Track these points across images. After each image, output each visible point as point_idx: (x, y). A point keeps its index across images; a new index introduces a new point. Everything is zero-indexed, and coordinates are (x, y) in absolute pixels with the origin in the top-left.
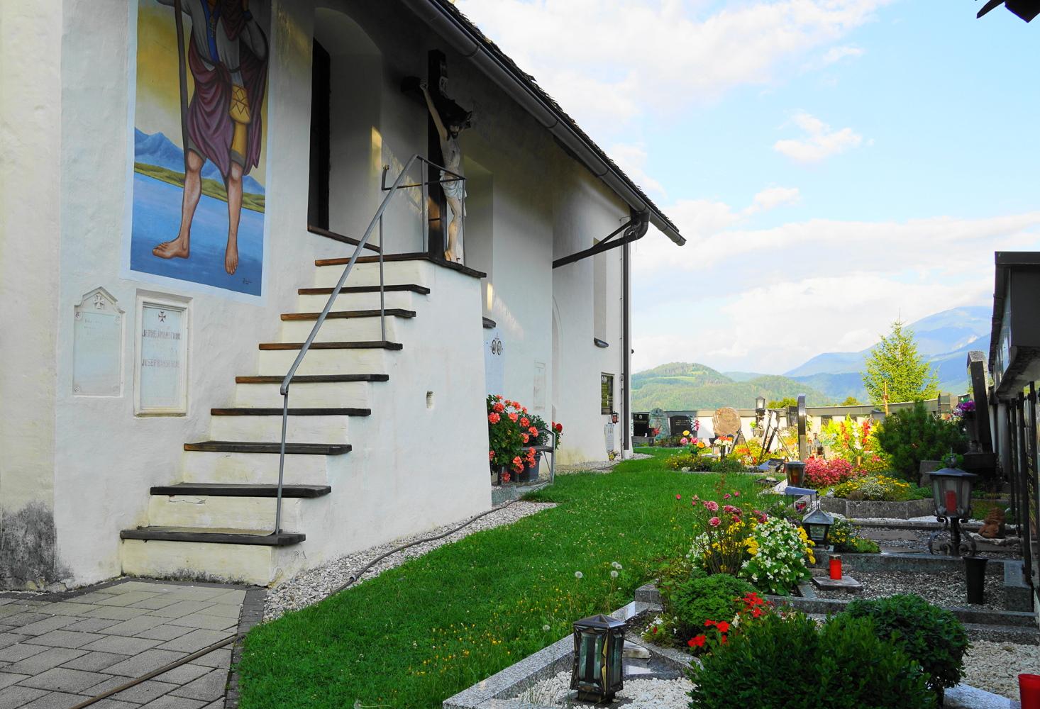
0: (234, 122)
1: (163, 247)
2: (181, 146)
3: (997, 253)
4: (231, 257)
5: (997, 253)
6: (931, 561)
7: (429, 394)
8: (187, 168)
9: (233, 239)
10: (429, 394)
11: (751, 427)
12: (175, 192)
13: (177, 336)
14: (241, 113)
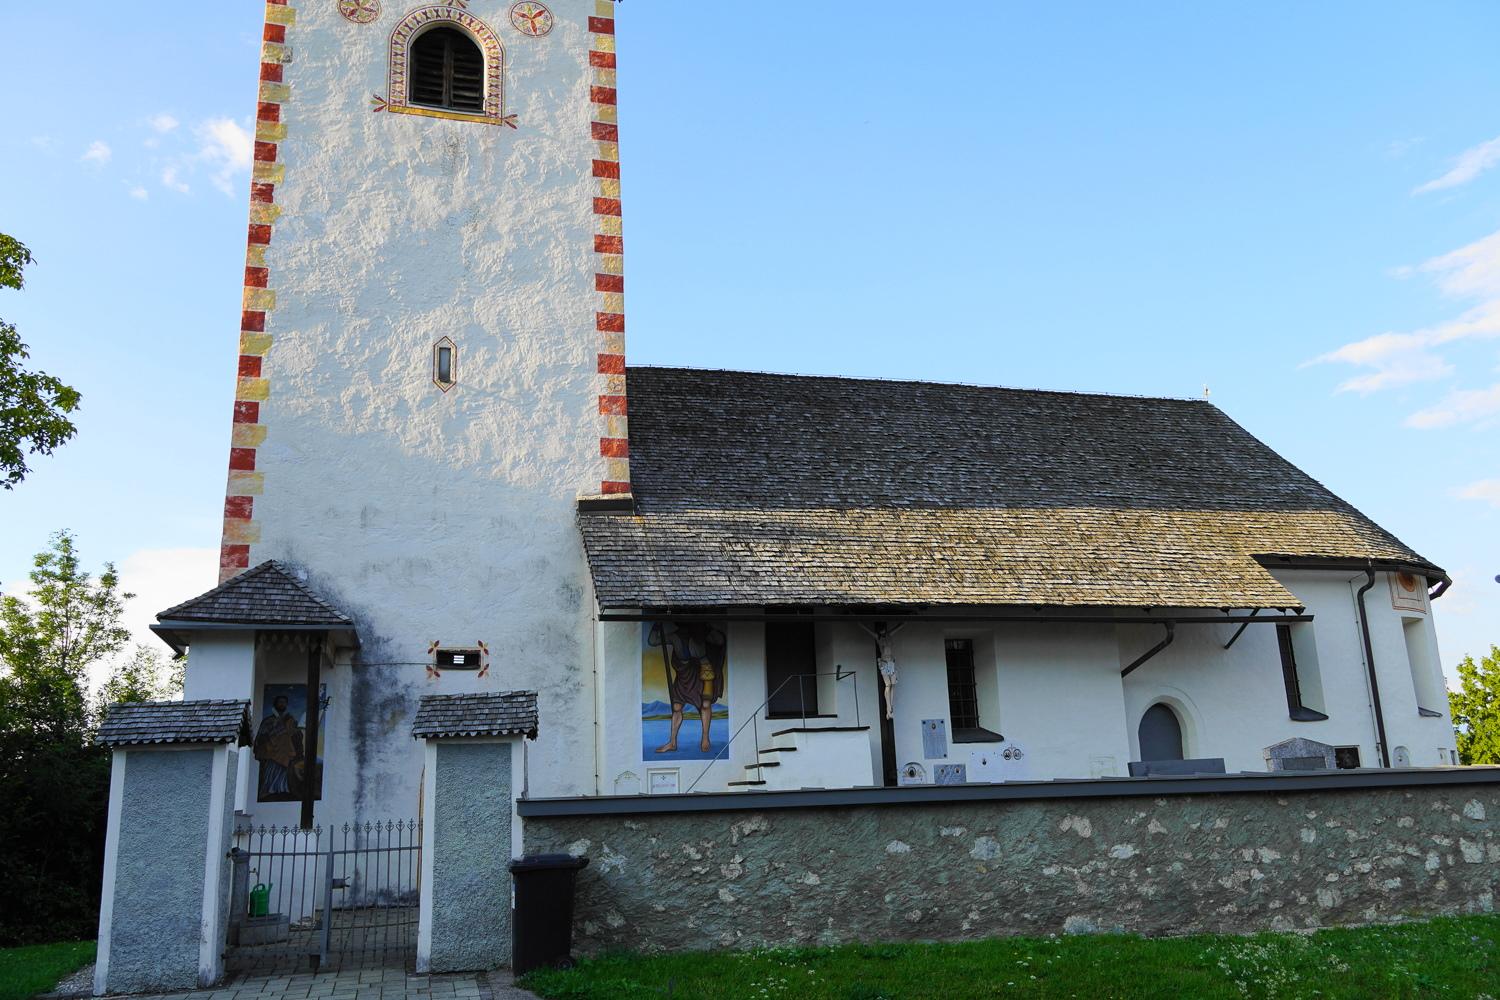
0: (703, 682)
1: (661, 748)
2: (669, 703)
3: (1222, 759)
4: (705, 743)
5: (1222, 759)
6: (979, 427)
7: (984, 763)
8: (673, 711)
9: (705, 736)
10: (984, 763)
11: (1375, 745)
12: (668, 724)
13: (674, 785)
14: (707, 675)
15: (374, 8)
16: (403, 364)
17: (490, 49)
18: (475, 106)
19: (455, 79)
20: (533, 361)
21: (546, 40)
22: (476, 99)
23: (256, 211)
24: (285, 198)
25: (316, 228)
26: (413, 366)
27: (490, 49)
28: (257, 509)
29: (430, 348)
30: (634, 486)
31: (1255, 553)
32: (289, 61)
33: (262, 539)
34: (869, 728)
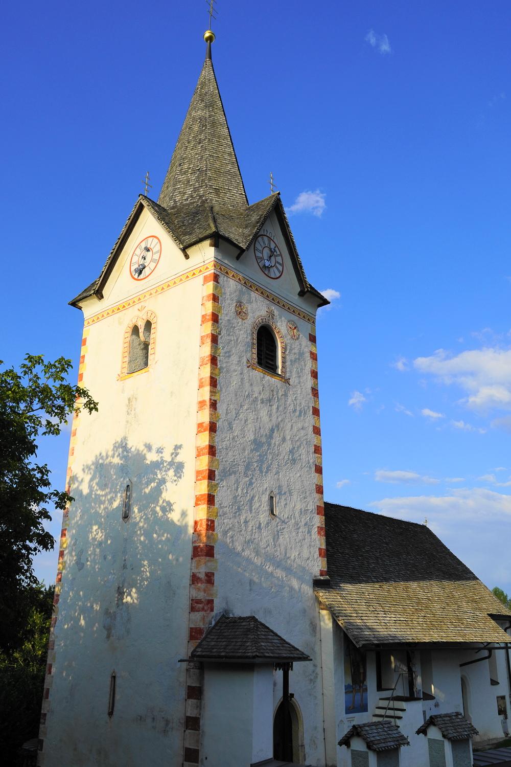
2: (352, 684)
15: (246, 312)
16: (260, 504)
17: (282, 343)
18: (272, 369)
19: (266, 353)
20: (298, 507)
21: (297, 341)
22: (273, 365)
23: (211, 414)
24: (221, 408)
25: (231, 428)
26: (263, 505)
27: (282, 343)
28: (216, 578)
29: (268, 497)
30: (329, 572)
31: (489, 613)
32: (220, 334)
33: (218, 596)
34: (179, 661)
